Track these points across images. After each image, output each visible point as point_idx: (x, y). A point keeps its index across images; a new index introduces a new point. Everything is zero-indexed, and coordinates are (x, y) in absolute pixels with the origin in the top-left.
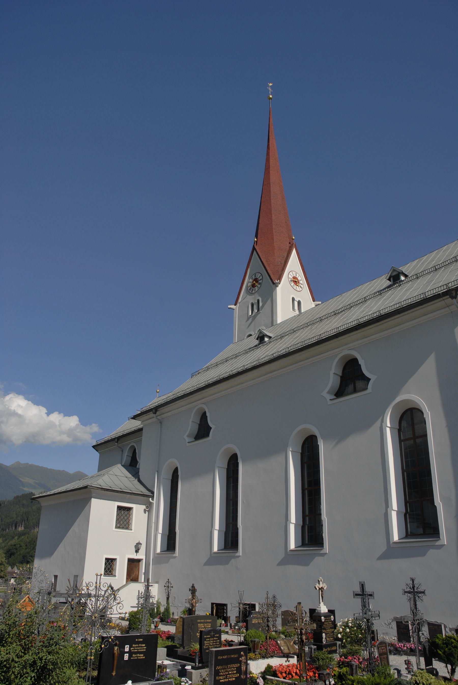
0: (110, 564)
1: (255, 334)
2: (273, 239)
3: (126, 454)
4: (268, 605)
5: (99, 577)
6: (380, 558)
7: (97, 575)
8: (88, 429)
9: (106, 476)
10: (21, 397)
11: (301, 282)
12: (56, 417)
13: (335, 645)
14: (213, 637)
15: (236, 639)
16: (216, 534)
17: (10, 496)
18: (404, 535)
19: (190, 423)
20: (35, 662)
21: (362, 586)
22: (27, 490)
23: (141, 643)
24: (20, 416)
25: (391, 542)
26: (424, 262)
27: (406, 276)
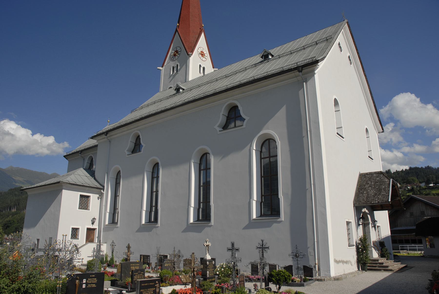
0: (75, 232)
1: (174, 86)
2: (189, 25)
3: (86, 161)
4: (175, 256)
5: (64, 237)
6: (244, 228)
7: (63, 236)
8: (61, 145)
9: (73, 175)
10: (12, 122)
11: (206, 55)
12: (38, 137)
13: (215, 277)
14: (140, 273)
15: (154, 275)
16: (144, 213)
17: (6, 189)
18: (260, 215)
19: (129, 142)
20: (19, 289)
21: (233, 245)
22: (18, 185)
23: (94, 277)
24: (12, 135)
25: (252, 219)
26: (284, 48)
27: (272, 56)
